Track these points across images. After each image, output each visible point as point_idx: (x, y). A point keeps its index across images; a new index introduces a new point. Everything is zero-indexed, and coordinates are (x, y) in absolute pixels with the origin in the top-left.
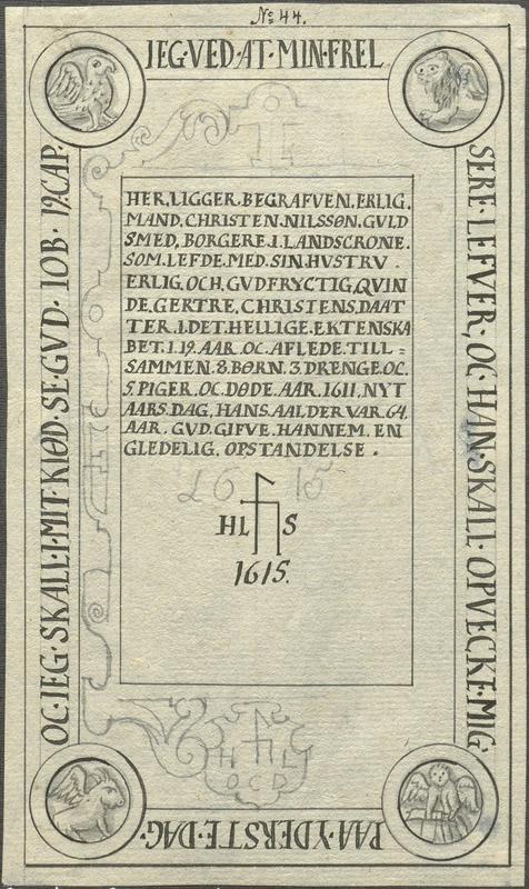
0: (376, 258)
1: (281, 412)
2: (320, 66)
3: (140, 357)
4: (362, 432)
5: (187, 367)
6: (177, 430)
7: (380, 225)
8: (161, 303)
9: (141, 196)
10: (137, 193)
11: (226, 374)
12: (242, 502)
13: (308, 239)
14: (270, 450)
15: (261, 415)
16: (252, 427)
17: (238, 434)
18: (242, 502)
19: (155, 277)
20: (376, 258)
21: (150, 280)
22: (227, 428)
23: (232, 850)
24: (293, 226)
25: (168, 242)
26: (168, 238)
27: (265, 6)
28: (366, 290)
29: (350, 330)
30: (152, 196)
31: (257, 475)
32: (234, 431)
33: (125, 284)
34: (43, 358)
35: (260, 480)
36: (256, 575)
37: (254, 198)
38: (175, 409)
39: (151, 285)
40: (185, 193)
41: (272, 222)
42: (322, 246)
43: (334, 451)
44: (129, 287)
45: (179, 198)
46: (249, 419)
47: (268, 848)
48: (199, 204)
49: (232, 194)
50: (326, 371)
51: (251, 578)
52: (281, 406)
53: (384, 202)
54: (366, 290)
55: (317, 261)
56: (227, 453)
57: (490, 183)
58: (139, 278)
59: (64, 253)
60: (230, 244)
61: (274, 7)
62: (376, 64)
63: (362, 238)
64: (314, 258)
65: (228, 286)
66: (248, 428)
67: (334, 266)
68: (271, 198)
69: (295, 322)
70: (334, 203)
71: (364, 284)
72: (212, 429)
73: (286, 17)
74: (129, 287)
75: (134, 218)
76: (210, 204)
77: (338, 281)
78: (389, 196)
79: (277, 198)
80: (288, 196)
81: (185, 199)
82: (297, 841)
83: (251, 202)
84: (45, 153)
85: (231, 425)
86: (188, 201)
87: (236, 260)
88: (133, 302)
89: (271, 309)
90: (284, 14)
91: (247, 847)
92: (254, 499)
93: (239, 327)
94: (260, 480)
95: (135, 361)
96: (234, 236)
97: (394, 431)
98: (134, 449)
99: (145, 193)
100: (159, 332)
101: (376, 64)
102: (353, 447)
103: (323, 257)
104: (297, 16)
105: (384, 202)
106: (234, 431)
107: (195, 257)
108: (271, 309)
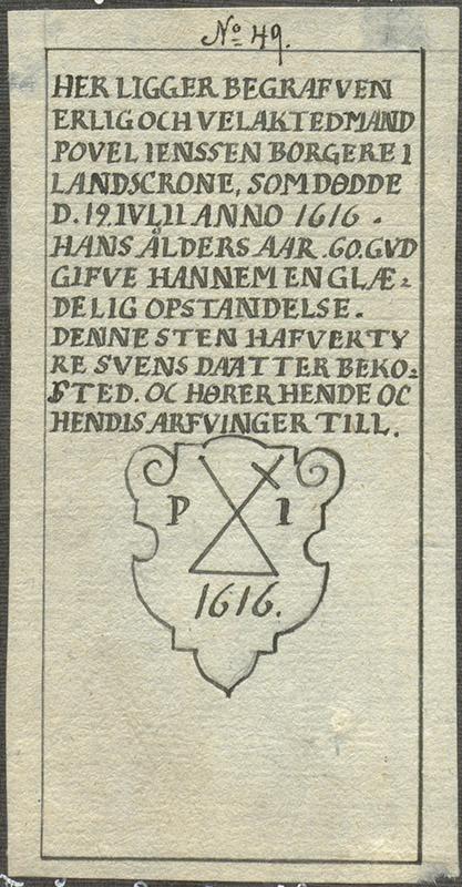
2: (201, 386)
13: (88, 180)
15: (197, 159)
16: (124, 361)
17: (88, 284)
22: (72, 274)
23: (262, 53)
25: (57, 339)
26: (267, 306)
31: (191, 571)
32: (83, 279)
33: (52, 123)
35: (270, 570)
36: (226, 605)
37: (241, 84)
38: (201, 366)
39: (88, 124)
42: (398, 126)
43: (305, 310)
44: (57, 127)
45: (129, 88)
46: (103, 261)
69: (274, 80)
73: (263, 36)
74: (57, 127)
79: (279, 86)
81: (137, 87)
83: (239, 90)
85: (78, 269)
86: (142, 91)
88: (272, 306)
90: (259, 31)
91: (319, 315)
94: (270, 570)
95: (263, 175)
96: (185, 79)
97: (247, 309)
98: (344, 279)
102: (331, 305)
104: (277, 32)
106: (83, 279)
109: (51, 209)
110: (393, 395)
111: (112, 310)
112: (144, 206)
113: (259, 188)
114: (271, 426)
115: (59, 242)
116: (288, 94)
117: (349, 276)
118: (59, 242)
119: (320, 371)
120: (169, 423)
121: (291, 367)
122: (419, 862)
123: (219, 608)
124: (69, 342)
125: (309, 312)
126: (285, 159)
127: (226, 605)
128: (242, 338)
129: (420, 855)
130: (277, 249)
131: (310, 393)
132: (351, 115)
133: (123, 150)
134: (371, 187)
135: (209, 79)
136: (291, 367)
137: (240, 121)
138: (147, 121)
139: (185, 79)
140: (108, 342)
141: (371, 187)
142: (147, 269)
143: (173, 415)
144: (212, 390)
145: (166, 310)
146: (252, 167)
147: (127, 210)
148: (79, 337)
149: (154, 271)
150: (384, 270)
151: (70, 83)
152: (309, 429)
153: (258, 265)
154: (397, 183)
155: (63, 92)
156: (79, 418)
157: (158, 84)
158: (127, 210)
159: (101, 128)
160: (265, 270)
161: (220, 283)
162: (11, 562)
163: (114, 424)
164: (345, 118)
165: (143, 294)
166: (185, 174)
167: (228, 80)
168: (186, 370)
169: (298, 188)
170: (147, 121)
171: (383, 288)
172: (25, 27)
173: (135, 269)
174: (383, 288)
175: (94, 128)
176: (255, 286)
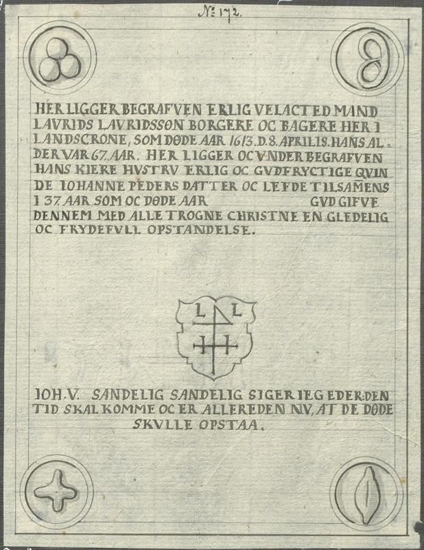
1: (71, 202)
5: (354, 126)
7: (324, 206)
9: (46, 106)
10: (43, 104)
12: (237, 346)
18: (237, 346)
28: (362, 175)
30: (53, 106)
31: (60, 197)
37: (130, 107)
47: (150, 233)
48: (87, 113)
52: (186, 197)
54: (362, 175)
57: (187, 185)
58: (292, 169)
60: (216, 158)
61: (218, 6)
62: (237, 313)
65: (340, 204)
66: (176, 107)
68: (326, 156)
69: (213, 152)
70: (191, 111)
71: (360, 171)
72: (337, 202)
77: (335, 170)
79: (331, 156)
80: (224, 137)
82: (153, 185)
83: (313, 158)
84: (303, 144)
87: (155, 140)
89: (247, 218)
92: (212, 322)
93: (349, 127)
96: (102, 104)
98: (329, 158)
99: (49, 104)
100: (227, 159)
101: (237, 313)
102: (241, 230)
107: (288, 169)
108: (247, 218)
109: (33, 214)
112: (263, 105)
121: (321, 187)
122: (234, 314)
123: (237, 143)
124: (265, 412)
125: (143, 218)
126: (251, 183)
127: (239, 142)
129: (407, 533)
130: (189, 201)
136: (321, 187)
137: (370, 218)
139: (102, 104)
141: (280, 158)
142: (222, 335)
144: (156, 199)
145: (169, 200)
148: (291, 156)
149: (38, 165)
151: (349, 124)
152: (207, 203)
155: (152, 157)
156: (226, 184)
157: (88, 107)
159: (144, 219)
161: (64, 218)
162: (7, 265)
165: (181, 178)
166: (129, 205)
167: (124, 105)
169: (87, 217)
173: (251, 121)
175: (209, 174)
176: (82, 219)
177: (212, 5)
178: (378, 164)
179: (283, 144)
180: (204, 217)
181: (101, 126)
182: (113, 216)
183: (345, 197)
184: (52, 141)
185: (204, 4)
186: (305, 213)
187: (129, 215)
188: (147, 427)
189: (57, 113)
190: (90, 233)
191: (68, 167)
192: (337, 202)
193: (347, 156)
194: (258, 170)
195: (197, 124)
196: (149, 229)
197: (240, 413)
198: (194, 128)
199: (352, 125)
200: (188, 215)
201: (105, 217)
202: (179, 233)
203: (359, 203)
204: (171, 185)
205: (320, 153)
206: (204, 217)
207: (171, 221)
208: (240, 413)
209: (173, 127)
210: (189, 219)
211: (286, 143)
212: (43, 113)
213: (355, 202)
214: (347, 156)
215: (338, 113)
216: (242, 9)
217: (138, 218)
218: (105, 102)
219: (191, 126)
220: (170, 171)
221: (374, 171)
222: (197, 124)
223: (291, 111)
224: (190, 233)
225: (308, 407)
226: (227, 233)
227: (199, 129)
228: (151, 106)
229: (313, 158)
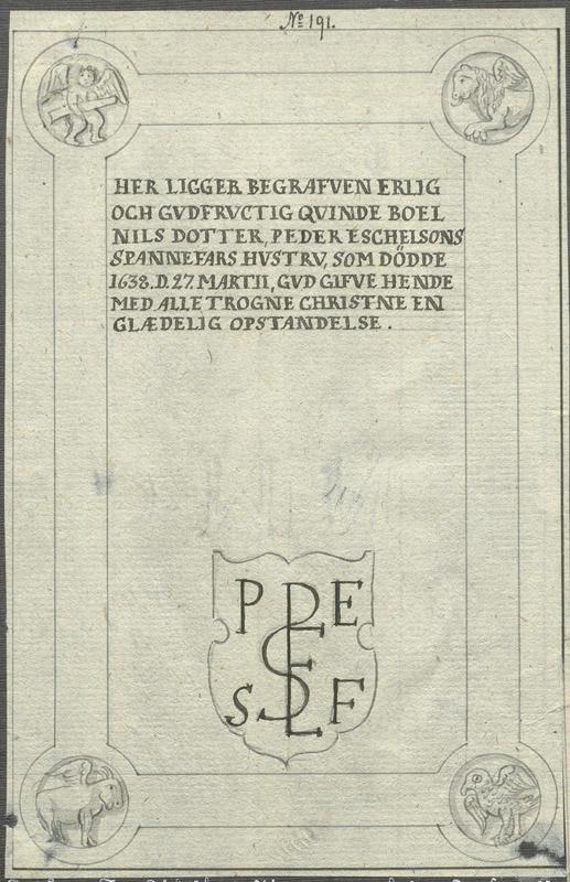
0: (315, 254)
3: (360, 312)
4: (213, 283)
6: (283, 283)
8: (305, 302)
11: (148, 290)
13: (148, 256)
14: (281, 323)
19: (409, 182)
20: (315, 254)
21: (404, 186)
24: (366, 193)
27: (294, 12)
29: (293, 262)
34: (262, 716)
37: (259, 185)
40: (183, 181)
41: (174, 260)
45: (177, 186)
47: (149, 299)
49: (298, 182)
50: (401, 190)
51: (123, 285)
53: (415, 188)
54: (309, 217)
55: (254, 257)
56: (232, 327)
59: (305, 669)
61: (306, 13)
63: (397, 209)
64: (250, 255)
66: (356, 282)
67: (272, 264)
69: (209, 180)
72: (318, 281)
75: (120, 304)
76: (331, 287)
78: (420, 182)
79: (287, 184)
83: (257, 189)
88: (386, 257)
93: (394, 282)
97: (305, 323)
103: (261, 253)
105: (415, 188)
110: (248, 303)
111: (183, 188)
113: (367, 325)
114: (215, 190)
115: (118, 182)
116: (335, 240)
117: (333, 280)
118: (118, 182)
119: (234, 190)
120: (215, 259)
126: (124, 217)
128: (384, 213)
131: (181, 323)
132: (361, 255)
133: (430, 212)
134: (411, 261)
135: (258, 231)
138: (193, 237)
140: (366, 278)
143: (219, 253)
146: (336, 248)
147: (258, 256)
150: (150, 319)
153: (201, 273)
154: (442, 259)
158: (258, 256)
160: (208, 277)
163: (414, 261)
164: (357, 257)
168: (278, 262)
170: (193, 237)
171: (149, 330)
172: (32, 32)
174: (149, 330)
177: (301, 12)
178: (363, 195)
179: (288, 326)
180: (265, 306)
181: (170, 188)
182: (133, 304)
183: (134, 207)
184: (147, 261)
185: (289, 12)
186: (416, 298)
187: (157, 302)
188: (335, 240)
189: (252, 241)
190: (319, 327)
191: (337, 262)
192: (318, 281)
193: (317, 184)
194: (165, 211)
195: (235, 302)
196: (115, 324)
197: (331, 242)
198: (395, 217)
199: (398, 280)
200: (239, 302)
201: (122, 306)
202: (276, 327)
203: (302, 185)
204: (226, 257)
205: (269, 181)
206: (265, 306)
207: (368, 310)
208: (331, 242)
209: (357, 262)
210: (240, 308)
211: (313, 188)
212: (332, 218)
213: (321, 187)
214: (317, 184)
215: (204, 284)
216: (339, 17)
217: (169, 307)
218: (376, 204)
219: (392, 214)
220: (314, 262)
221: (329, 210)
222: (400, 211)
223: (424, 189)
224: (291, 328)
225: (320, 256)
226: (190, 329)
227: (431, 242)
228: (294, 185)
229: (257, 189)
